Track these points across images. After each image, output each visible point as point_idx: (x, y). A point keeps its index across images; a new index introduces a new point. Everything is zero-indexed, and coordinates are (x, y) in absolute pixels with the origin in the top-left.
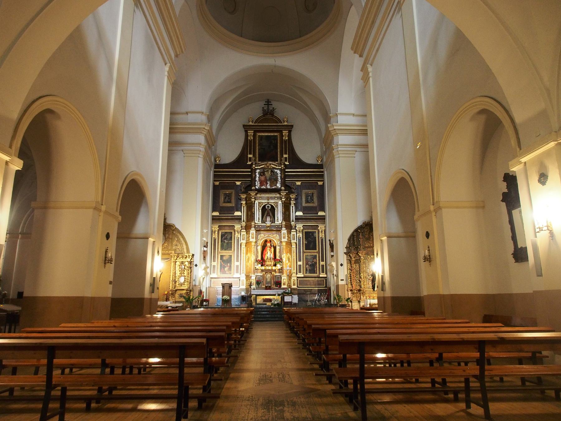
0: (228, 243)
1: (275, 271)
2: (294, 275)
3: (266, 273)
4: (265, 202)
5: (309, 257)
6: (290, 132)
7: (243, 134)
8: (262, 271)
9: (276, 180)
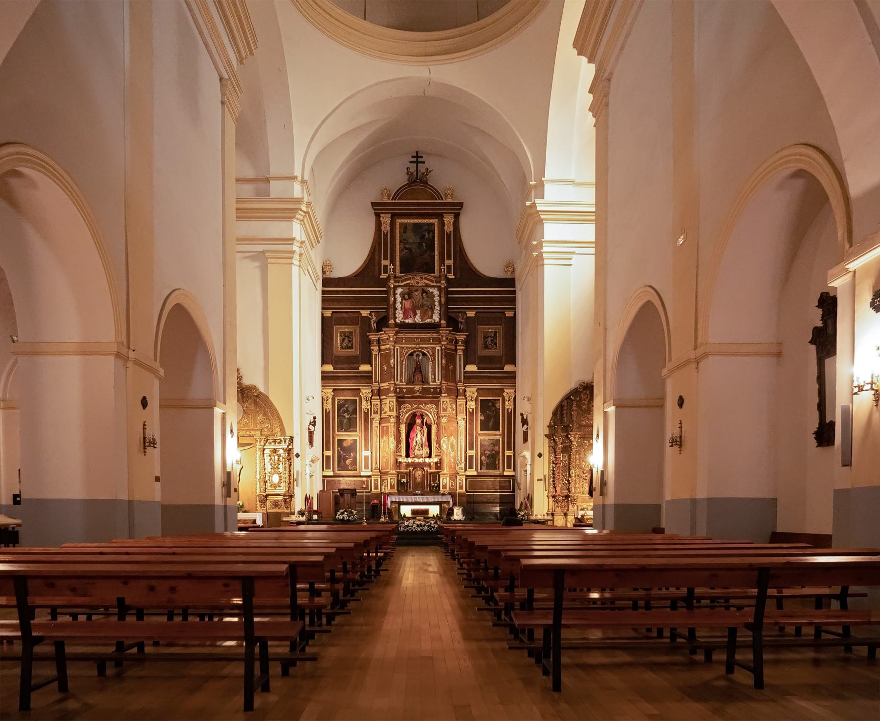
0: (349, 419)
1: (429, 465)
4: (412, 349)
5: (486, 443)
6: (457, 216)
7: (373, 218)
8: (408, 465)
9: (431, 308)
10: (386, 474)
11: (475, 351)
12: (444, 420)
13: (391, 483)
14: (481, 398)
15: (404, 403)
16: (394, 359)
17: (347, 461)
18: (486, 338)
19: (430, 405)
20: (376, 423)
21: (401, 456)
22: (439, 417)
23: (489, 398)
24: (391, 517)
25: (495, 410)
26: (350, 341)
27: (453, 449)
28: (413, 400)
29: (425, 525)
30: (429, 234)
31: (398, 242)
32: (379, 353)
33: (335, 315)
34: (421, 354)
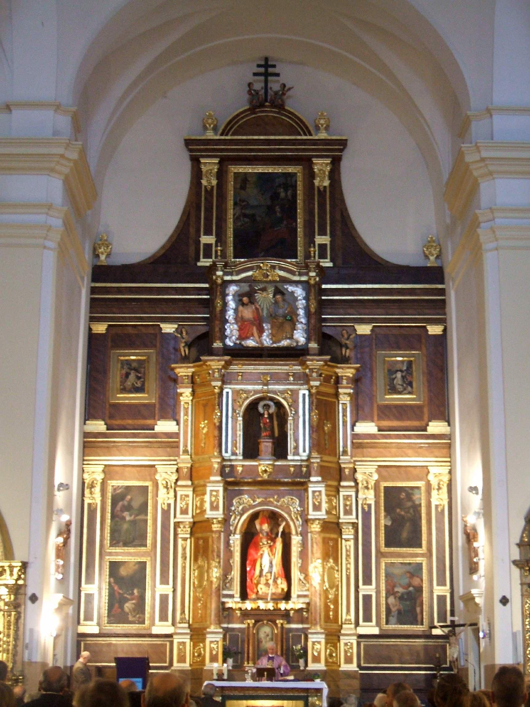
1: (286, 615)
2: (348, 629)
3: (257, 622)
4: (256, 392)
5: (397, 571)
6: (336, 162)
8: (246, 614)
13: (211, 650)
14: (384, 484)
26: (139, 378)
30: (286, 191)
31: (230, 203)
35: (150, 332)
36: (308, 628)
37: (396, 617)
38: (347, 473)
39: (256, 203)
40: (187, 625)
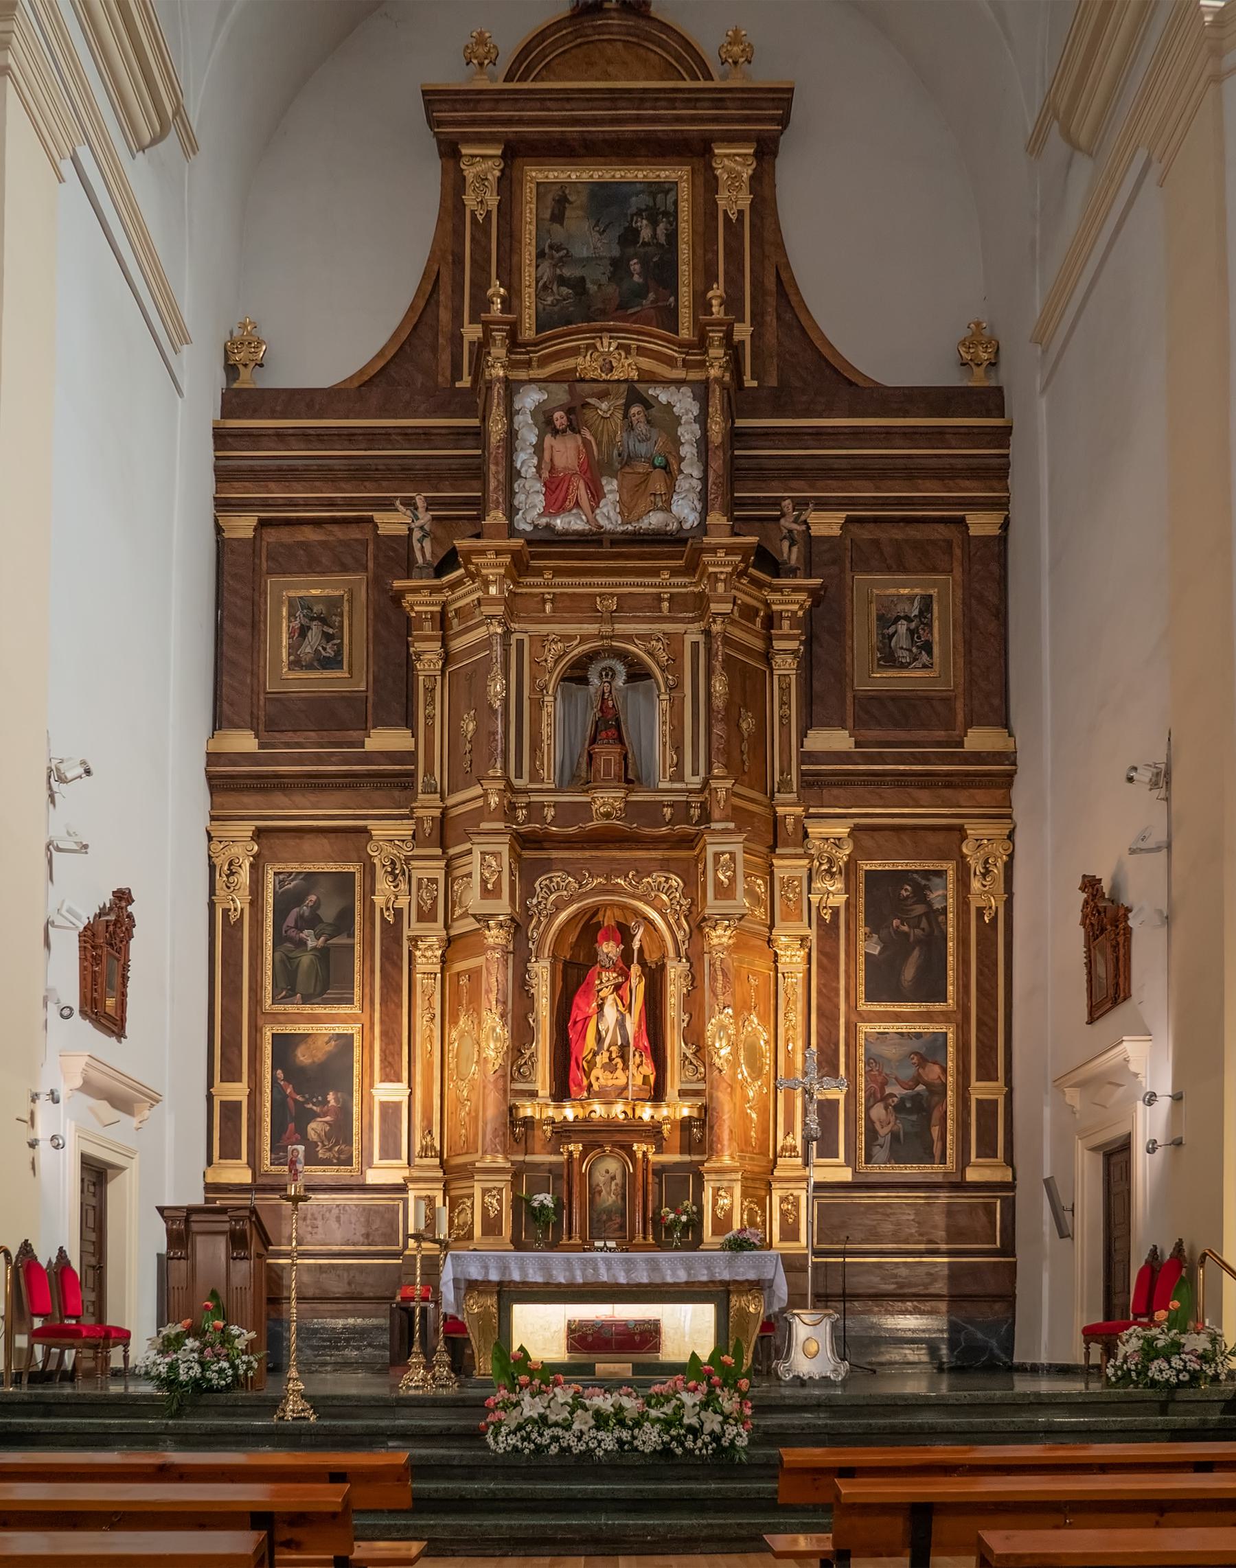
0: (323, 954)
1: (653, 1133)
2: (788, 1165)
4: (584, 639)
5: (890, 1051)
6: (766, 151)
7: (432, 172)
8: (563, 1132)
9: (666, 468)
10: (467, 1172)
11: (841, 677)
12: (720, 937)
13: (485, 1210)
14: (867, 865)
15: (546, 866)
16: (507, 677)
17: (312, 1125)
18: (886, 621)
19: (658, 877)
20: (427, 960)
21: (533, 1094)
22: (699, 926)
23: (901, 865)
24: (461, 1364)
25: (926, 914)
26: (328, 637)
27: (756, 1072)
28: (587, 854)
29: (643, 1416)
30: (654, 223)
31: (528, 253)
32: (443, 671)
33: (271, 535)
34: (620, 668)
35: (353, 537)
36: (702, 1163)
37: (887, 1145)
38: (790, 828)
39: (585, 253)
40: (437, 1161)
